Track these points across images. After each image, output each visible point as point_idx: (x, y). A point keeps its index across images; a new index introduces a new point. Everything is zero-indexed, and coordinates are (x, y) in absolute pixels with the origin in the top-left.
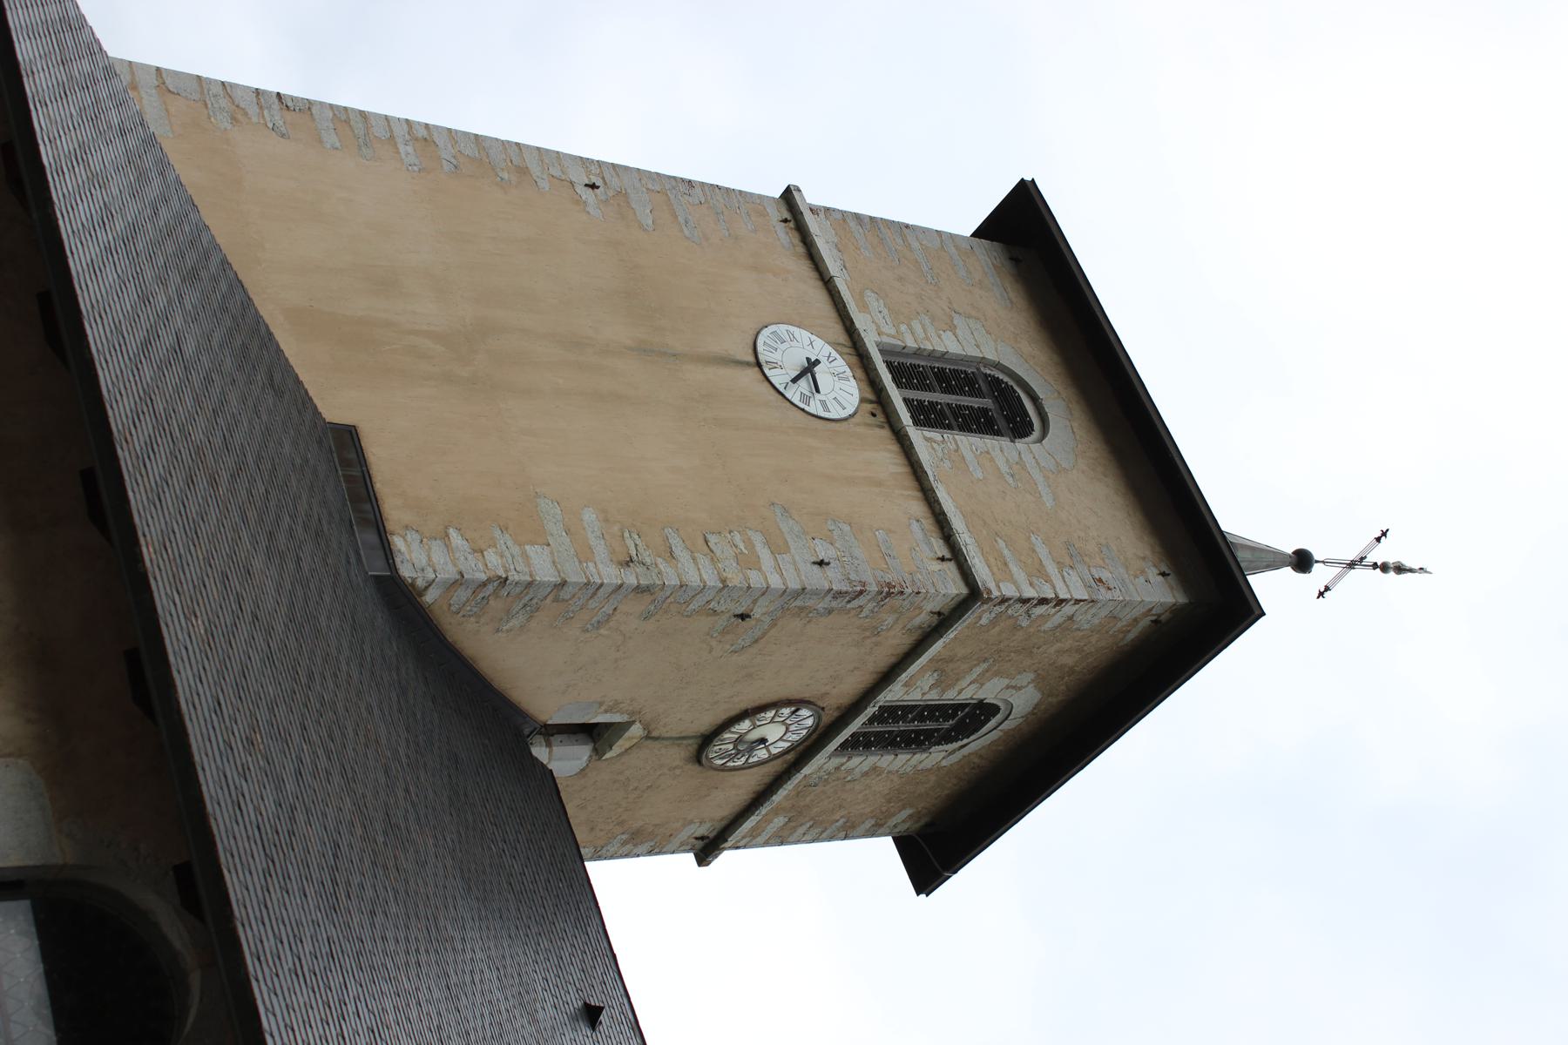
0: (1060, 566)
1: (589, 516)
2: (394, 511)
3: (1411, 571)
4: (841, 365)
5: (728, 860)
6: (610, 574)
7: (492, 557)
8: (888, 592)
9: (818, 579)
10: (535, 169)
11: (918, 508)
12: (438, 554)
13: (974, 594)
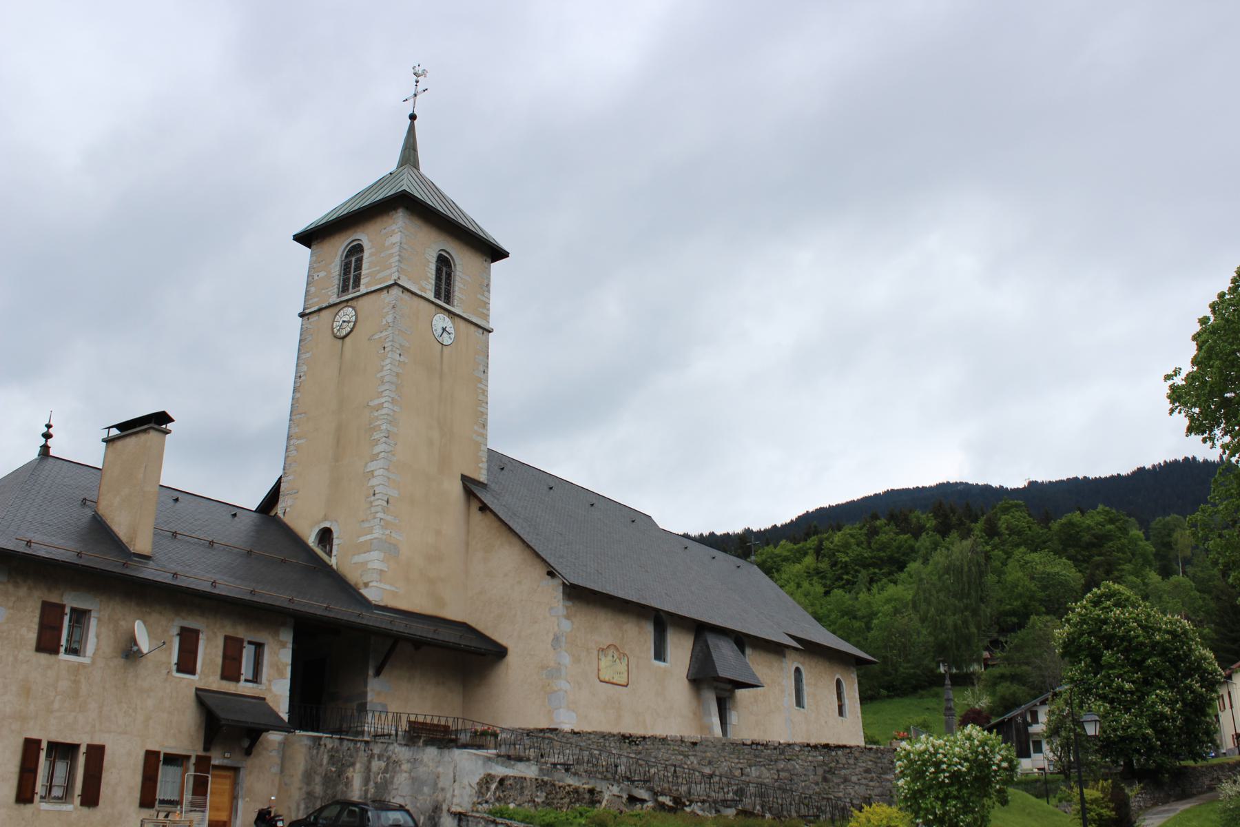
3: (411, 131)
11: (472, 328)
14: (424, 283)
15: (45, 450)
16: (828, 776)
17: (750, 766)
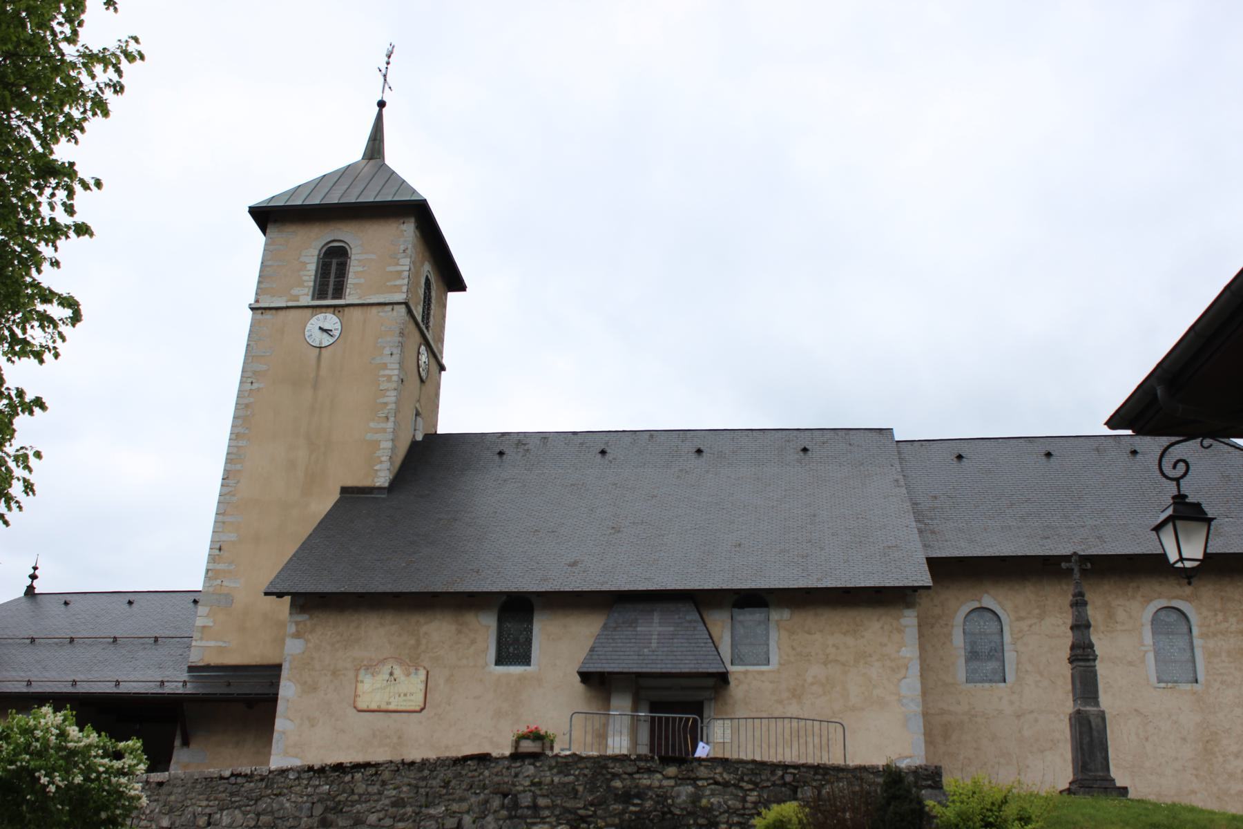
0: (398, 264)
1: (372, 425)
2: (367, 483)
3: (380, 117)
4: (321, 316)
5: (445, 362)
6: (390, 425)
7: (384, 459)
8: (402, 334)
9: (396, 357)
10: (246, 401)
11: (374, 310)
12: (382, 474)
13: (406, 304)
14: (295, 291)
15: (30, 591)
16: (331, 816)
17: (222, 810)
